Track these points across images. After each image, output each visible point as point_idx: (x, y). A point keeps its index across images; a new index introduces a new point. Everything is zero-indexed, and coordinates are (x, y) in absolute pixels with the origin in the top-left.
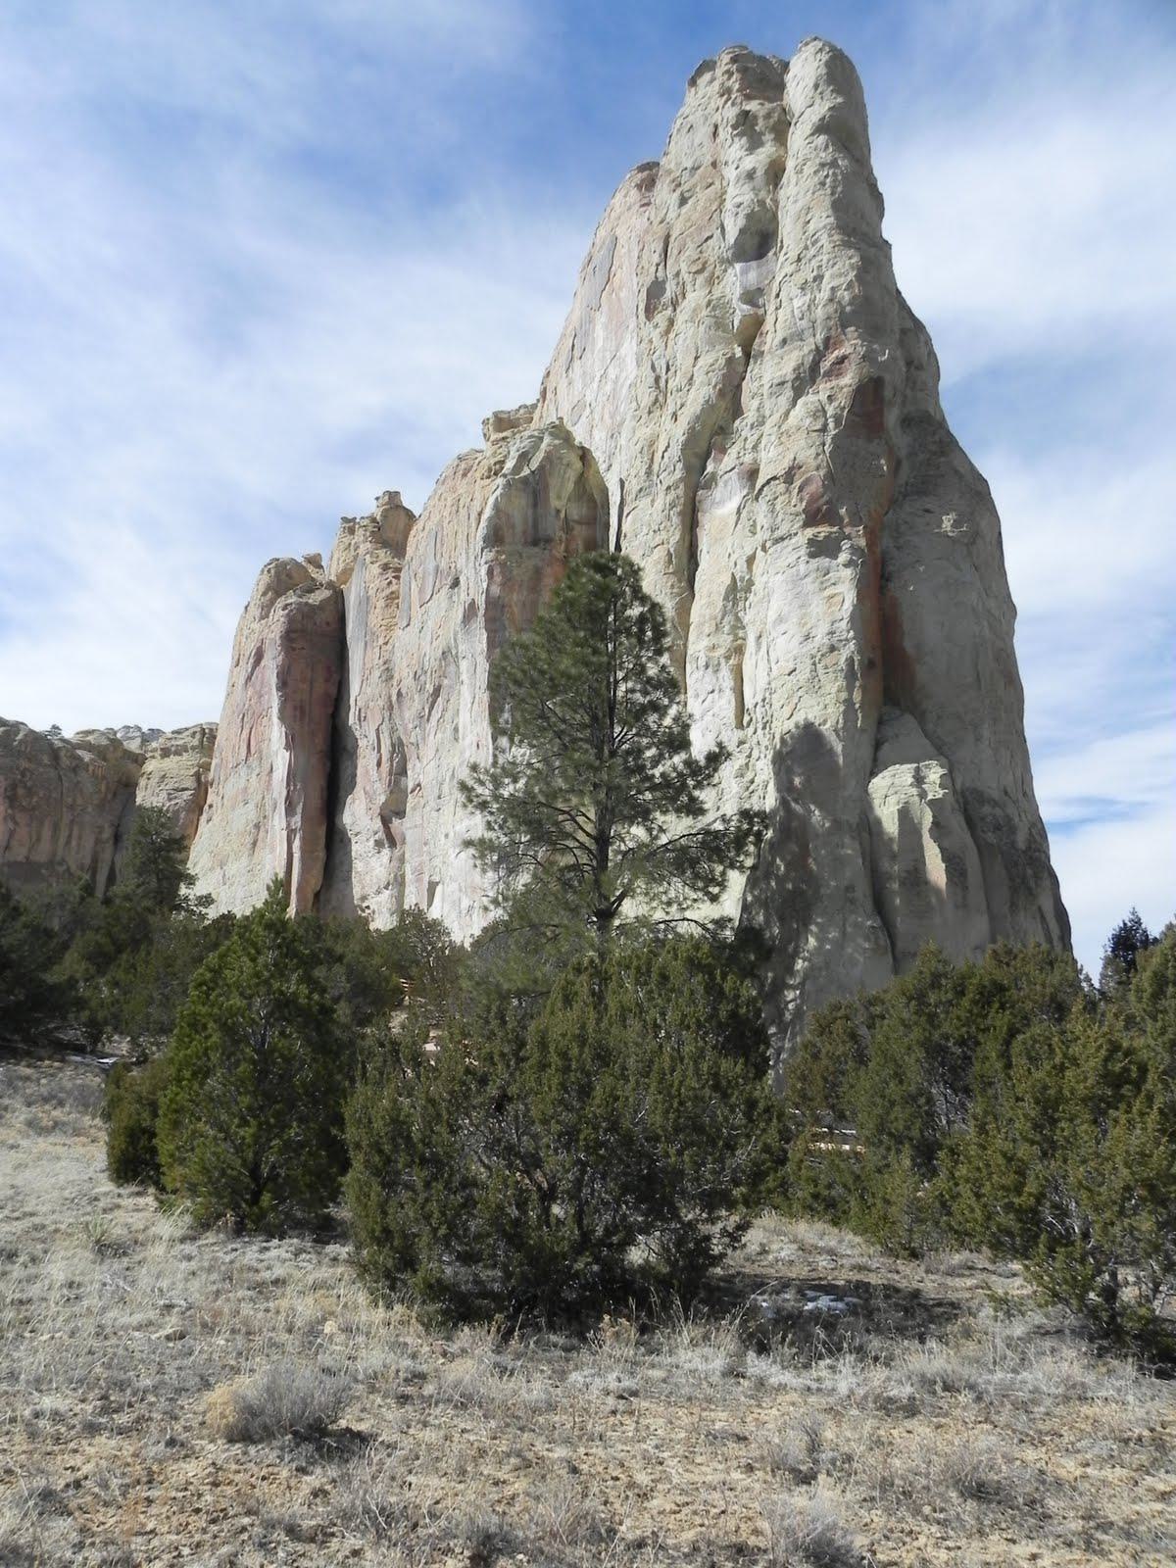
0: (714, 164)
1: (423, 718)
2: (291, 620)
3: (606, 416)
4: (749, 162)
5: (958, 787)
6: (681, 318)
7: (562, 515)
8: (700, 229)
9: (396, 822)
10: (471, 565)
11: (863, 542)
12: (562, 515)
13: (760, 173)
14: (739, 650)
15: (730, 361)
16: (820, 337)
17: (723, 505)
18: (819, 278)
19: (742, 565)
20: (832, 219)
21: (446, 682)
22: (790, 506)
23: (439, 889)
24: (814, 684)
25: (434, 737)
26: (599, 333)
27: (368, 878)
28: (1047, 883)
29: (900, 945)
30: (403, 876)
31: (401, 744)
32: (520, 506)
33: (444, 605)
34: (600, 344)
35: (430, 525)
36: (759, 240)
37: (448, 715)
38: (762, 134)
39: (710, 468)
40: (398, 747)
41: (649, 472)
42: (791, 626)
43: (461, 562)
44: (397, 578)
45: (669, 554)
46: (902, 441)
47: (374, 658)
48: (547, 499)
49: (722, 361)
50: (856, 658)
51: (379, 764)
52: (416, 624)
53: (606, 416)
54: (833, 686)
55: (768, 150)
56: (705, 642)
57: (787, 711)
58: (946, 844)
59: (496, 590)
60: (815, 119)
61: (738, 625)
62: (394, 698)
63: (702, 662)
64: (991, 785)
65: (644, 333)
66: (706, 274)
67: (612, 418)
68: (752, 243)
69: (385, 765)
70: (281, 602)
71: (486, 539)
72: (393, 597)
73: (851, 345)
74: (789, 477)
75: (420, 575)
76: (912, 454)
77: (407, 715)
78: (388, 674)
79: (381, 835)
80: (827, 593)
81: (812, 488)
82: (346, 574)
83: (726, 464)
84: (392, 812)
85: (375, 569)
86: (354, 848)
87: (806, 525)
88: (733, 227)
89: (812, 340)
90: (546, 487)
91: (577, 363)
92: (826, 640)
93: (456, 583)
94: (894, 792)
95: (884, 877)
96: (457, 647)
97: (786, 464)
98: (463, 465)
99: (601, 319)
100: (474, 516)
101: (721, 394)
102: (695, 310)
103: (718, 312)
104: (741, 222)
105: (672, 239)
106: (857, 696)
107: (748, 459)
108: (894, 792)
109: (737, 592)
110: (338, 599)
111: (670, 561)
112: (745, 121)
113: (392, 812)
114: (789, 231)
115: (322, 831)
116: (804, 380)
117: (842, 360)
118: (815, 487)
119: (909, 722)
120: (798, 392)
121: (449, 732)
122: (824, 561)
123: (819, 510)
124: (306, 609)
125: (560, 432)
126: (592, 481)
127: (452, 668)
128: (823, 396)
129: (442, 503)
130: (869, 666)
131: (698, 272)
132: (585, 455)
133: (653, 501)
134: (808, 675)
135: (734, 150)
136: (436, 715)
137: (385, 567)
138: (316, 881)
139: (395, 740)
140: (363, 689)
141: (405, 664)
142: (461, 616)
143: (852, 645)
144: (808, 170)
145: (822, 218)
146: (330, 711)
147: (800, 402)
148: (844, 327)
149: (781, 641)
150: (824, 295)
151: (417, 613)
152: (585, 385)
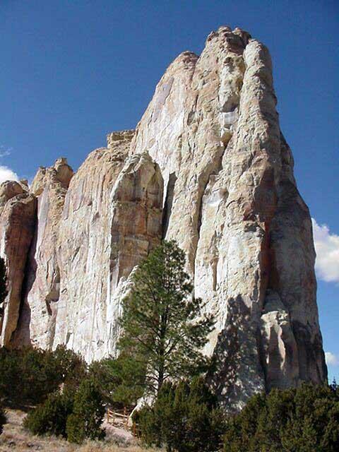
0: (216, 72)
1: (70, 260)
2: (14, 209)
3: (164, 148)
4: (230, 77)
5: (292, 320)
6: (200, 128)
7: (145, 190)
8: (210, 96)
9: (52, 304)
10: (99, 197)
11: (264, 229)
12: (145, 190)
13: (234, 82)
14: (216, 260)
15: (219, 147)
16: (253, 151)
17: (213, 203)
18: (253, 129)
19: (219, 227)
20: (258, 108)
21: (82, 246)
22: (239, 213)
23: (72, 336)
24: (243, 280)
25: (75, 268)
26: (164, 113)
27: (37, 327)
28: (320, 356)
29: (268, 376)
30: (54, 329)
31: (58, 269)
32: (129, 185)
33: (84, 212)
34: (164, 118)
35: (81, 177)
36: (232, 105)
37: (82, 261)
38: (234, 67)
39: (208, 187)
40: (57, 270)
41: (185, 185)
42: (236, 256)
43: (94, 195)
44: (64, 197)
45: (191, 219)
46: (280, 190)
47: (50, 231)
48: (139, 183)
49: (215, 147)
50: (259, 271)
51: (47, 277)
52: (71, 218)
53: (164, 148)
54: (250, 280)
55: (237, 73)
56: (203, 256)
57: (233, 288)
58: (286, 342)
59: (116, 219)
60: (255, 71)
61: (216, 251)
62: (58, 250)
63: (202, 264)
64: (303, 320)
65: (186, 129)
66: (211, 113)
67: (167, 148)
68: (229, 106)
69: (50, 279)
70: (10, 201)
71: (114, 197)
72: (60, 205)
73: (263, 155)
74: (239, 201)
75: (75, 197)
76: (282, 196)
77: (63, 258)
78: (55, 238)
79: (45, 309)
80: (251, 246)
81: (246, 207)
82: (40, 191)
83: (215, 187)
84: (53, 297)
85: (54, 191)
86: (32, 313)
87: (245, 220)
88: (223, 100)
89: (249, 151)
90: (140, 178)
91: (153, 124)
92: (249, 264)
93: (91, 204)
94: (272, 320)
95: (264, 345)
96: (89, 231)
97: (238, 196)
98: (98, 154)
99: (164, 108)
100: (101, 177)
101: (214, 160)
102: (206, 126)
103: (215, 128)
104: (226, 99)
105: (199, 97)
106: (259, 286)
107: (223, 187)
108: (272, 320)
109: (216, 238)
110: (36, 201)
111: (191, 221)
112: (229, 60)
113: (53, 297)
114: (243, 104)
115: (18, 304)
116: (247, 165)
117: (260, 160)
118: (248, 206)
119: (276, 295)
120: (244, 170)
121: (82, 269)
122: (250, 234)
123: (249, 215)
124: (20, 205)
125: (147, 156)
126: (158, 177)
127: (86, 240)
128: (253, 173)
129: (87, 169)
130: (263, 274)
131: (209, 111)
132: (156, 166)
133: (186, 196)
134: (242, 276)
135: (224, 70)
136: (76, 260)
137: (58, 191)
138: (14, 326)
139: (55, 268)
140: (42, 243)
141: (64, 235)
142: (92, 218)
143: (258, 266)
144: (252, 88)
145: (255, 108)
146: (26, 251)
147: (244, 173)
148: (262, 148)
149: (232, 261)
150: (255, 136)
151: (72, 213)
152: (156, 133)
